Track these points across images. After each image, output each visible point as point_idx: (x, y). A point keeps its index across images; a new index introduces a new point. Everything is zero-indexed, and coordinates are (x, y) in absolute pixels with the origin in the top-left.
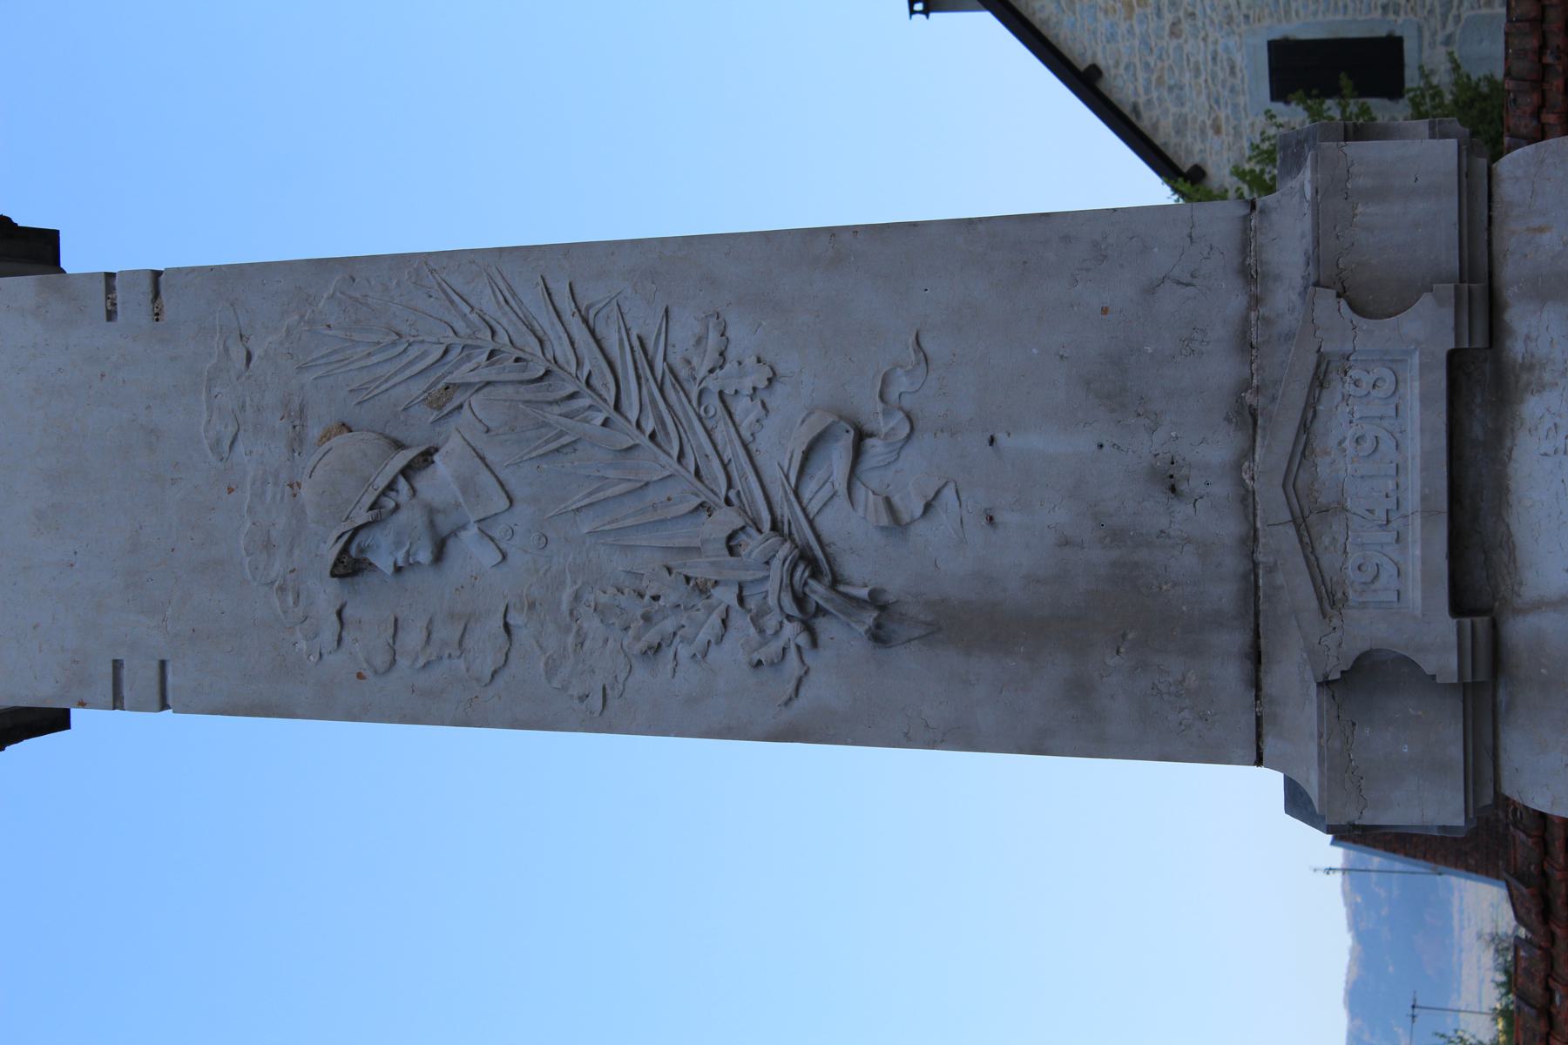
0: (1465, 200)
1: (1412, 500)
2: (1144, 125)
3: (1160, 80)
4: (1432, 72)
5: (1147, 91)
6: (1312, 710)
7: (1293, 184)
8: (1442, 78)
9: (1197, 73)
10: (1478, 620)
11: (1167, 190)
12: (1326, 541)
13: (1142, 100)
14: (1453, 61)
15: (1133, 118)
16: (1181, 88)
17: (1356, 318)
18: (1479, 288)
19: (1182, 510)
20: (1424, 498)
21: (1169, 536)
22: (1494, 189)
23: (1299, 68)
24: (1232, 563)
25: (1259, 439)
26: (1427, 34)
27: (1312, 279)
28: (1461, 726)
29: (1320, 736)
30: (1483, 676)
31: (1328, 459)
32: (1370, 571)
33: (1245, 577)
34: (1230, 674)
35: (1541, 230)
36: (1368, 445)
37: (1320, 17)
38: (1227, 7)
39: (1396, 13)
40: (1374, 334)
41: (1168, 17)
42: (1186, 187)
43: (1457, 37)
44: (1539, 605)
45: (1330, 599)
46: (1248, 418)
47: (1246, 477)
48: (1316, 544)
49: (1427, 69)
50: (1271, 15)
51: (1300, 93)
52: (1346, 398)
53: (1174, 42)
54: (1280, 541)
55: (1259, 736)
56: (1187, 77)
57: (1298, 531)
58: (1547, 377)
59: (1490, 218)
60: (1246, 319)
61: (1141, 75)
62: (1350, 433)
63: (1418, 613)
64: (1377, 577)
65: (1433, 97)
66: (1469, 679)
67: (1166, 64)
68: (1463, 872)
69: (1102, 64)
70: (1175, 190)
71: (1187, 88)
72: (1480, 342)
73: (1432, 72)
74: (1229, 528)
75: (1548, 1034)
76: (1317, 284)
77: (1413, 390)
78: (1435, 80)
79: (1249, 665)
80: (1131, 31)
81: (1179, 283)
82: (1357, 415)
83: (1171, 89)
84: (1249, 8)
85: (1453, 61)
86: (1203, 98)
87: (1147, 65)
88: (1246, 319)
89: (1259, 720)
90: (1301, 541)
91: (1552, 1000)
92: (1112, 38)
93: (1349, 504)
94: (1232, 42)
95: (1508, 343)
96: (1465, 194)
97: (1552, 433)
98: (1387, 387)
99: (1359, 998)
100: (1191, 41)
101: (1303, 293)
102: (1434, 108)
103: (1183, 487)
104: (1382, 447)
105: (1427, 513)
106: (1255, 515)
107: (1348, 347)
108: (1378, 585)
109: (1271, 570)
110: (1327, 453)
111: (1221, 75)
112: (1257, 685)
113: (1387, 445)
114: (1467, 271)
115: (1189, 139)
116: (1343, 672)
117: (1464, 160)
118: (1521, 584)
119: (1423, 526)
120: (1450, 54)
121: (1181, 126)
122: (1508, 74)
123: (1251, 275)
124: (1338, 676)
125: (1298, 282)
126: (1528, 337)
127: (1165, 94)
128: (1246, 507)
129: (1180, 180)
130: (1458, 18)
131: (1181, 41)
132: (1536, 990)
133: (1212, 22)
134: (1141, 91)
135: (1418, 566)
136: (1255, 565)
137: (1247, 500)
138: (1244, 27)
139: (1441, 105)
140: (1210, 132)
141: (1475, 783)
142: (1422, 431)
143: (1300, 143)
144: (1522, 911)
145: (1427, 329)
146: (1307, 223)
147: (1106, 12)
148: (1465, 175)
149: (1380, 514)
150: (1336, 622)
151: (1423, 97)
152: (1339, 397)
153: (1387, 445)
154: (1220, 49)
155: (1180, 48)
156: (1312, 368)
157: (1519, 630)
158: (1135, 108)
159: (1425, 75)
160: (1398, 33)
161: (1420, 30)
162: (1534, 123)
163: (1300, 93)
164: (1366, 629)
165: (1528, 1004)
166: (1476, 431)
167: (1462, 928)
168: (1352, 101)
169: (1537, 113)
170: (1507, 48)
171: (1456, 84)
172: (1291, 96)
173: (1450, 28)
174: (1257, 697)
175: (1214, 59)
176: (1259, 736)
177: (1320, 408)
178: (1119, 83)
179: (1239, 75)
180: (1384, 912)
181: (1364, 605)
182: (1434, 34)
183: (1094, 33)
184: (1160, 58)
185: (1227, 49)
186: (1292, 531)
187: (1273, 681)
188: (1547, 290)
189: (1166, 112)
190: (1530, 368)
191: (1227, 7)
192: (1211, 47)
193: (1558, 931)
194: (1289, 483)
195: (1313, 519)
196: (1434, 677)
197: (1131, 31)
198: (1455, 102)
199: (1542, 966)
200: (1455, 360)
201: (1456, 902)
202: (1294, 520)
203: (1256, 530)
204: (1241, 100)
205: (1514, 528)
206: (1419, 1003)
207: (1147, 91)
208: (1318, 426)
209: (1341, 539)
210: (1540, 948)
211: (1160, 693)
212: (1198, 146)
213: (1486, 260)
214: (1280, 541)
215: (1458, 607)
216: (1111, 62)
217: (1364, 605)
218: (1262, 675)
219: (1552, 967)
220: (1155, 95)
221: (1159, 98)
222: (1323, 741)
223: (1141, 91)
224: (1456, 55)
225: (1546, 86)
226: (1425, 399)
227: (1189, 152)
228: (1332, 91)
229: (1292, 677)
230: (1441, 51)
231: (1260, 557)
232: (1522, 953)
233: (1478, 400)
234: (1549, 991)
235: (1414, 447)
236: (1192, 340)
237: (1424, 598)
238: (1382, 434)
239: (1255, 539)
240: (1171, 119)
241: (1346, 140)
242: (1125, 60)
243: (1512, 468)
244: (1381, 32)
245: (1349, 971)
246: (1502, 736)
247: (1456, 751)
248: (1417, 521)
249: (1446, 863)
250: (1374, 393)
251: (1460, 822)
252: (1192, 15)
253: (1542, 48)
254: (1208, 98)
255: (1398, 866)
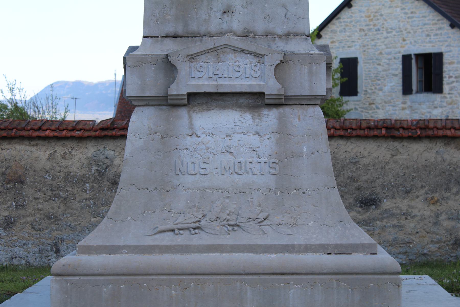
0: (308, 97)
1: (221, 82)
2: (334, 21)
3: (347, 26)
4: (347, 104)
5: (344, 22)
6: (159, 52)
7: (314, 48)
8: (345, 107)
9: (349, 37)
10: (186, 100)
11: (315, 27)
12: (209, 57)
13: (341, 20)
14: (350, 110)
15: (336, 18)
16: (345, 32)
17: (275, 66)
18: (283, 101)
19: (219, 15)
20: (222, 85)
21: (211, 11)
22: (311, 106)
23: (349, 67)
24: (203, 30)
25: (239, 38)
26: (358, 103)
27: (286, 53)
28: (155, 95)
29: (152, 55)
30: (170, 102)
31: (233, 57)
32: (201, 70)
33: (199, 33)
34: (170, 29)
35: (299, 119)
36: (237, 69)
37: (364, 72)
38: (368, 45)
39: (364, 94)
40: (270, 71)
41: (365, 28)
42: (316, 33)
43: (357, 112)
44: (190, 118)
45: (192, 58)
46: (245, 35)
47: (228, 34)
48: (208, 54)
49: (348, 103)
50: (365, 58)
51: (342, 66)
52: (251, 63)
53: (358, 30)
54: (209, 43)
55: (152, 37)
56: (348, 34)
57: (212, 49)
58: (257, 120)
59: (303, 104)
60: (275, 34)
61: (349, 20)
62: (241, 64)
63: (188, 83)
64: (199, 71)
65: (340, 105)
66: (169, 98)
67: (352, 28)
68: (115, 113)
69: (353, 8)
70: (315, 30)
71: (344, 33)
72: (267, 101)
73: (347, 104)
74: (213, 29)
75: (68, 130)
76: (285, 54)
77: (253, 82)
78: (345, 105)
79: (172, 34)
80: (362, 17)
81: (286, 14)
82: (246, 66)
83: (344, 29)
84: (367, 52)
85: (350, 110)
86: (341, 38)
87: (351, 22)
88: (275, 34)
89: (157, 37)
90: (209, 49)
91: (78, 131)
92: (360, 11)
93: (220, 63)
94: (358, 47)
95: (267, 110)
96: (310, 97)
97: (240, 122)
98: (254, 75)
99: (78, 85)
100: (358, 35)
101: (282, 50)
102: (337, 105)
103: (225, 15)
104: (237, 73)
105: (217, 86)
106: (217, 36)
107: (266, 63)
108: (196, 72)
109: (201, 41)
110: (235, 57)
111: (348, 43)
112: (167, 37)
113: (237, 75)
114: (287, 98)
115: (329, 34)
116: (171, 61)
117: (320, 97)
118: (197, 113)
119: (214, 85)
120: (352, 109)
121: (334, 32)
122: (345, 120)
123: (288, 36)
124: (170, 60)
125: (285, 49)
126: (268, 115)
127: (343, 27)
128: (219, 34)
129: (318, 31)
130: (362, 112)
131: (358, 32)
132: (80, 126)
133: (363, 41)
134: (344, 20)
135: (202, 83)
136: (202, 36)
137: (221, 34)
138: (362, 50)
139: (337, 107)
140: (331, 40)
141: (138, 99)
142: (241, 85)
143: (326, 51)
144: (103, 123)
145: (271, 87)
146: (302, 52)
147: (368, 10)
148: (315, 97)
149: (217, 72)
150: (186, 59)
151: (340, 102)
152: (251, 61)
153: (237, 75)
154: (356, 43)
155: (356, 31)
156: (260, 53)
157: (183, 112)
158: (339, 18)
159: (346, 102)
160: (358, 95)
161: (359, 101)
162: (331, 127)
163: (342, 66)
164: (183, 68)
165: (76, 124)
166: (242, 100)
167: (100, 114)
168: (339, 81)
169: (334, 128)
170: (353, 119)
171: (343, 111)
172: (341, 64)
173: (359, 109)
174: (163, 37)
175: (353, 42)
176: (152, 37)
177: (248, 55)
178: (347, 13)
179: (348, 49)
180: (104, 92)
181: (190, 67)
182: (358, 105)
183: (362, 6)
184: (354, 26)
185: (356, 45)
186: (212, 47)
187: (168, 41)
188: (281, 119)
189: (338, 27)
190: (259, 116)
191: (368, 45)
192: (356, 41)
193: (97, 133)
194: (226, 46)
195: (216, 53)
196: (170, 88)
197: (362, 17)
198: (338, 111)
199: (87, 128)
200: (262, 94)
201: (107, 112)
202: (215, 47)
203: (212, 36)
204: (341, 50)
205: (213, 111)
206: (77, 100)
207: (344, 22)
208: (243, 55)
209: (210, 61)
210: (93, 128)
211: (164, 8)
212: (327, 36)
213: (291, 103)
214: (209, 43)
215: (191, 95)
216: (353, 11)
217: (190, 67)
218: (170, 38)
219: (87, 131)
220: (343, 24)
221: (342, 25)
222: (150, 56)
223: (344, 20)
224: (352, 111)
225: (341, 130)
226: (251, 85)
227: (326, 34)
228: (342, 76)
229: (169, 46)
230: (353, 107)
231: (204, 38)
232: (91, 123)
233: (250, 101)
234: (81, 130)
235: (237, 82)
236: (269, 18)
237: (193, 85)
238: (240, 74)
239: (210, 36)
240: (336, 29)
241: (327, 64)
242: (353, 15)
243: (231, 111)
244: (359, 90)
245: (87, 82)
246: (153, 107)
247: (148, 94)
248: (215, 83)
249: (118, 108)
250: (252, 71)
251: (127, 95)
252: (366, 35)
253: (352, 129)
254: (342, 40)
255: (117, 96)
